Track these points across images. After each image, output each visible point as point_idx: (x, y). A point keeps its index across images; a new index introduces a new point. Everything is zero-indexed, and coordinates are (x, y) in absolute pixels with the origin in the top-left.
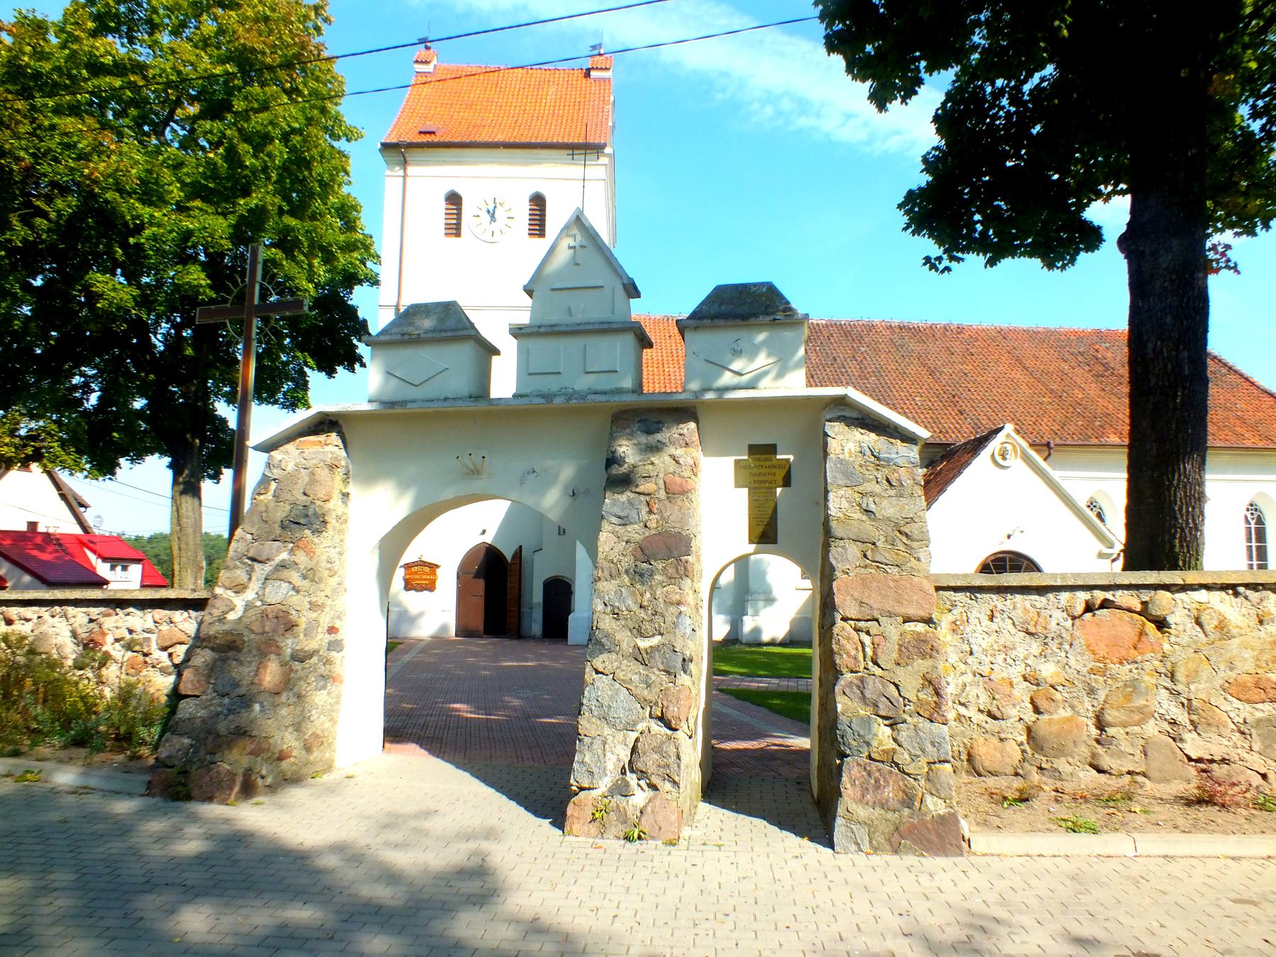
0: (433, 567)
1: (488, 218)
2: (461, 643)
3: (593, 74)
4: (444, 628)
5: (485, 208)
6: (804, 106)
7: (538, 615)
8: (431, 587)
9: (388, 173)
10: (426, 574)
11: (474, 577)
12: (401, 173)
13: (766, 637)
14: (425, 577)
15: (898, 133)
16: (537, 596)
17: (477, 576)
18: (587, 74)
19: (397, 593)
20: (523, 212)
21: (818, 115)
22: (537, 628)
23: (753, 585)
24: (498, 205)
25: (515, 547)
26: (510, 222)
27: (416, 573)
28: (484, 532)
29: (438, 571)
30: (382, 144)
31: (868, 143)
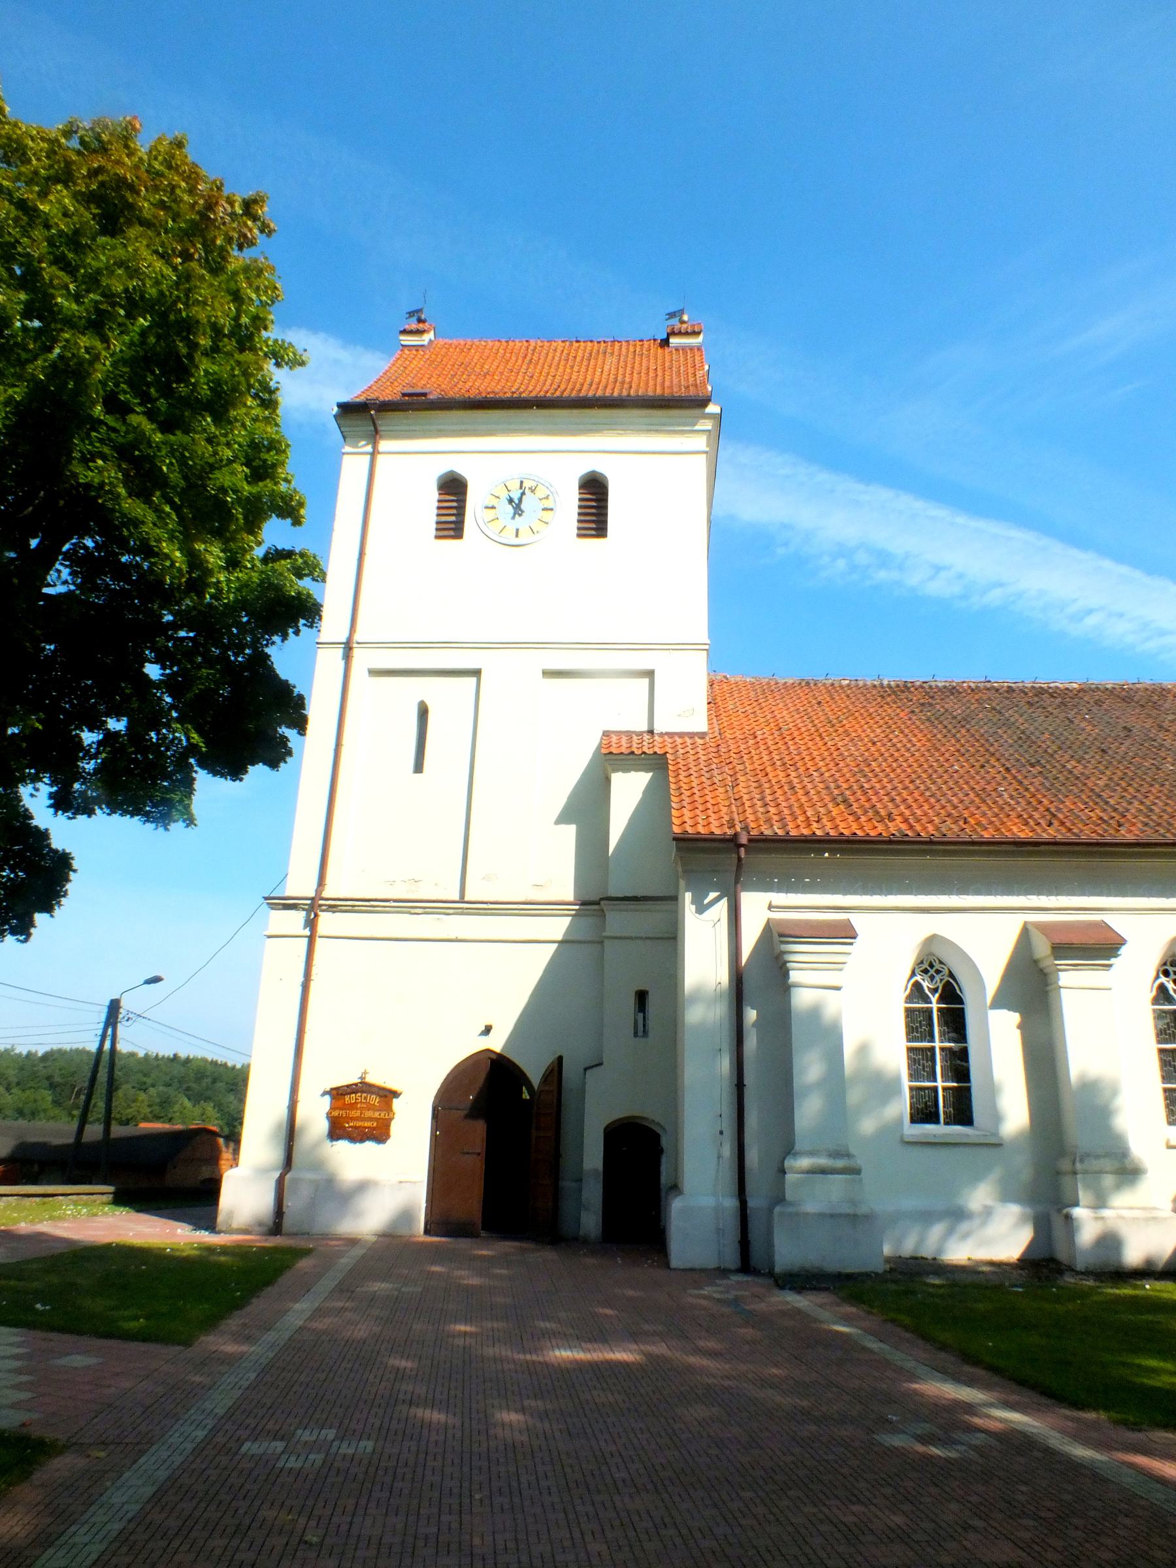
0: (388, 1095)
1: (510, 509)
2: (436, 1254)
3: (674, 341)
4: (405, 1216)
5: (504, 495)
6: (884, 558)
7: (593, 1193)
8: (380, 1133)
9: (347, 449)
10: (370, 1107)
11: (467, 1117)
12: (369, 448)
13: (1133, 1255)
14: (369, 1114)
15: (1001, 585)
16: (593, 1156)
17: (475, 1112)
18: (665, 343)
19: (317, 1145)
20: (570, 501)
21: (901, 568)
22: (591, 1222)
23: (1077, 1134)
24: (527, 491)
25: (547, 1060)
26: (547, 516)
27: (352, 1106)
28: (488, 1030)
29: (396, 1103)
30: (340, 405)
31: (964, 597)
